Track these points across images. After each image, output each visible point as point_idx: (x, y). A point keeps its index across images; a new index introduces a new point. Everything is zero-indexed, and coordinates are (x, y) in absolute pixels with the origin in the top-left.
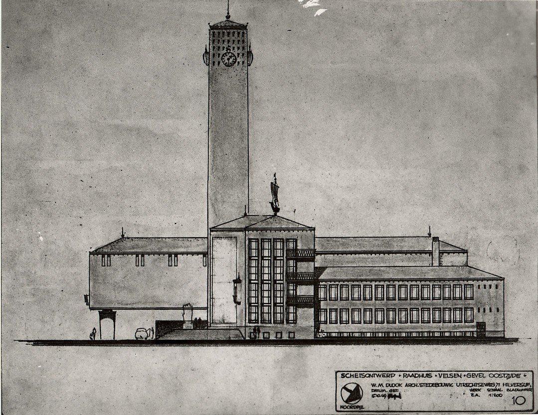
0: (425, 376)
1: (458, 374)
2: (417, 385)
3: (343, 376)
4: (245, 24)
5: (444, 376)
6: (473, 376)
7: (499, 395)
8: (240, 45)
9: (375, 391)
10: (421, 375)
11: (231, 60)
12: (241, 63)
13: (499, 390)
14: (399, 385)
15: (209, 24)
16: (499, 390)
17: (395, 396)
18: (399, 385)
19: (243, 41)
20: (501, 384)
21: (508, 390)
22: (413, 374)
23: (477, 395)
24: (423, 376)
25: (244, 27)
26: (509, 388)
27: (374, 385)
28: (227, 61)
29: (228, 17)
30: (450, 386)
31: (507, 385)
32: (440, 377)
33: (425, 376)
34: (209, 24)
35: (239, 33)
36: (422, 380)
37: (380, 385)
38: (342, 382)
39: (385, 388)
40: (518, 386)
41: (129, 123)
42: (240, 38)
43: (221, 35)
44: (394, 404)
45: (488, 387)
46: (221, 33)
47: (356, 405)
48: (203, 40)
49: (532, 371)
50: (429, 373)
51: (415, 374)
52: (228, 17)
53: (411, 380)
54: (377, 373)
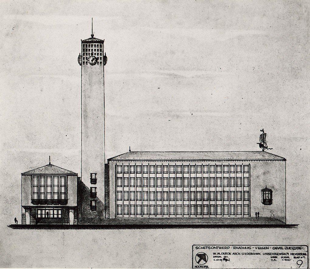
0: (247, 248)
1: (243, 247)
2: (240, 254)
3: (197, 248)
4: (103, 40)
5: (258, 248)
6: (276, 248)
7: (288, 260)
8: (99, 52)
9: (215, 257)
10: (244, 247)
11: (94, 61)
12: (99, 63)
13: (288, 257)
14: (230, 254)
15: (81, 40)
16: (288, 257)
17: (226, 260)
18: (230, 254)
19: (101, 50)
20: (290, 254)
21: (295, 257)
22: (239, 247)
23: (275, 260)
24: (245, 248)
25: (102, 42)
26: (295, 256)
27: (214, 254)
28: (91, 62)
29: (92, 36)
30: (259, 254)
31: (293, 254)
32: (256, 249)
33: (247, 248)
34: (81, 40)
35: (95, 45)
36: (245, 251)
37: (218, 253)
38: (196, 252)
39: (221, 255)
40: (299, 255)
41: (162, 76)
42: (99, 48)
43: (85, 46)
44: (228, 264)
45: (281, 256)
46: (91, 45)
47: (204, 265)
48: (78, 50)
49: (193, 246)
50: (281, 246)
51: (241, 247)
52: (92, 36)
53: (236, 251)
54: (219, 246)
